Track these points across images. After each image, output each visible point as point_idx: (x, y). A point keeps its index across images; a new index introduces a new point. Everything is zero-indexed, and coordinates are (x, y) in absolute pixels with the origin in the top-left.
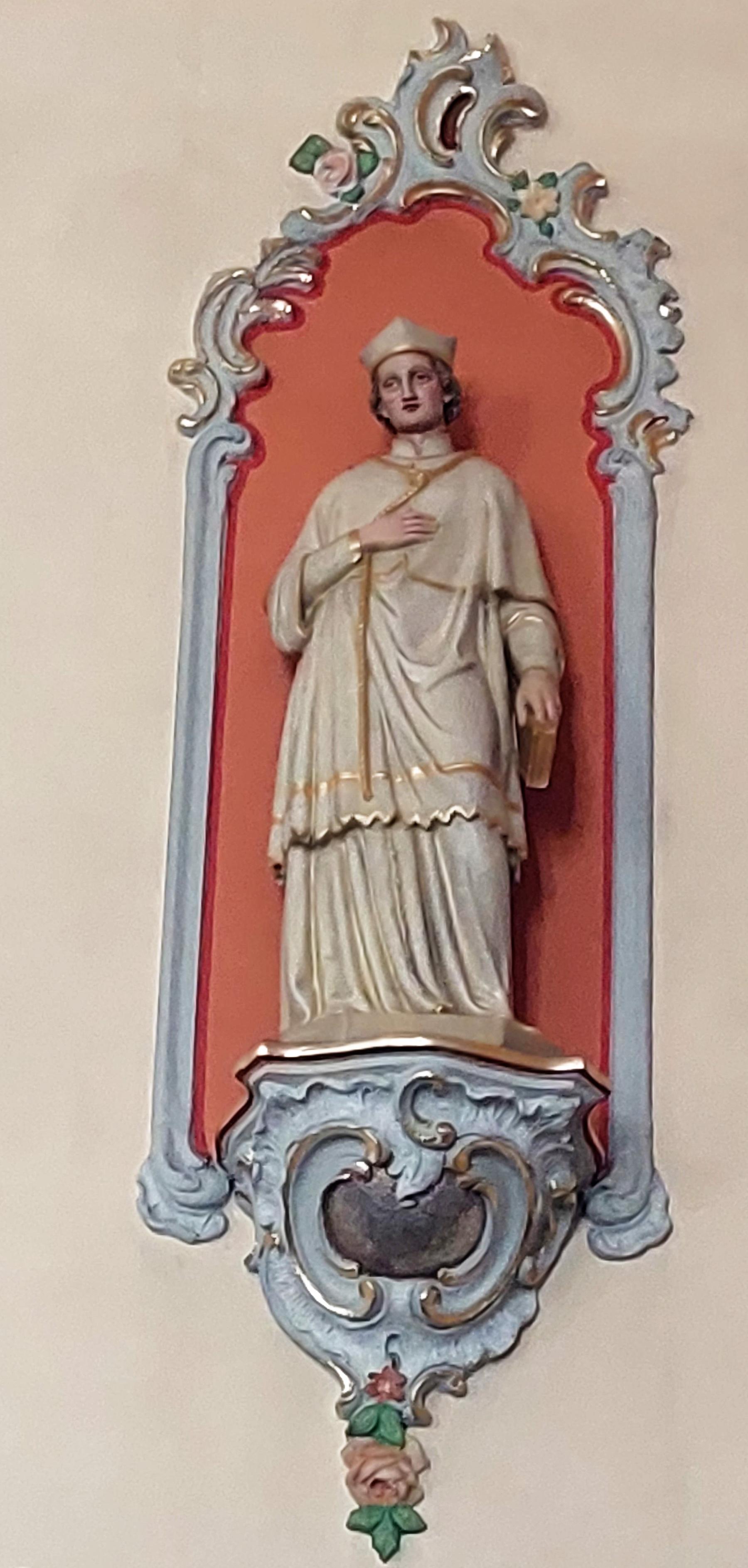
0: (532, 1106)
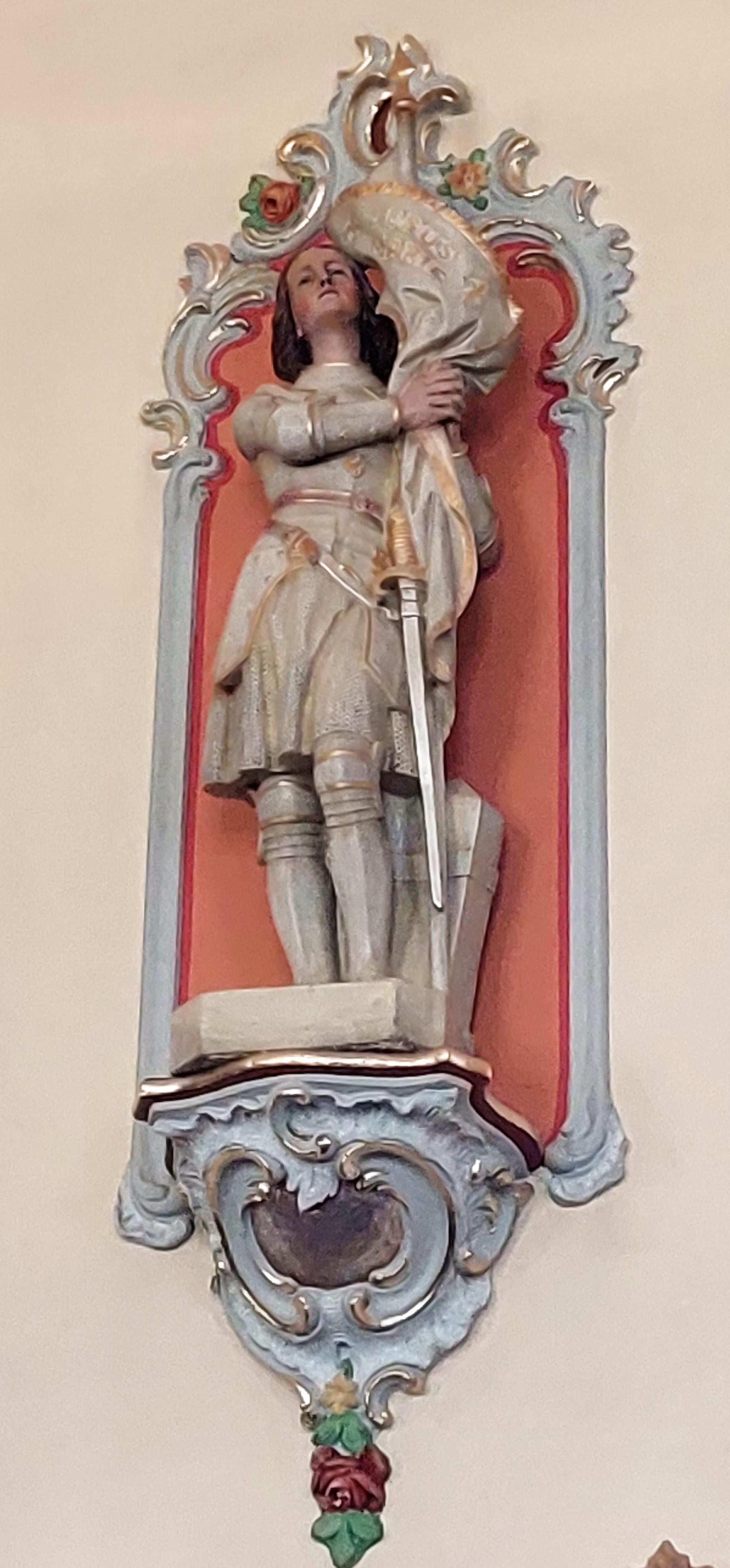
0: (405, 1105)
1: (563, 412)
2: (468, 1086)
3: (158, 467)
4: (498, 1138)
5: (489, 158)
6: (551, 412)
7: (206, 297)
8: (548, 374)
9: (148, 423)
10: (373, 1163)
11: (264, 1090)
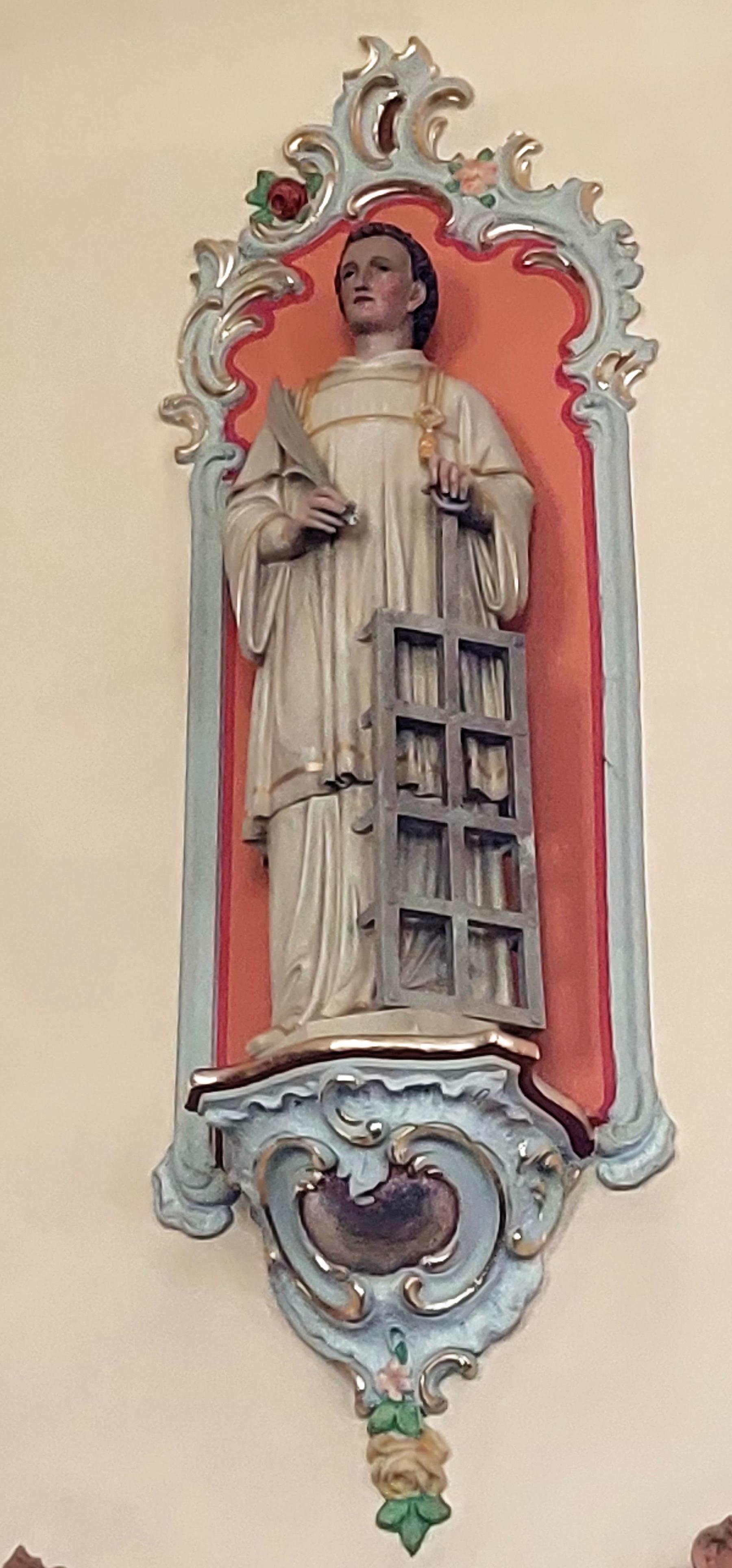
0: (452, 1088)
1: (587, 407)
2: (516, 1068)
3: (180, 462)
4: (543, 1119)
5: (496, 159)
6: (574, 408)
7: (218, 293)
8: (568, 369)
9: (167, 419)
10: (430, 1146)
11: (314, 1077)
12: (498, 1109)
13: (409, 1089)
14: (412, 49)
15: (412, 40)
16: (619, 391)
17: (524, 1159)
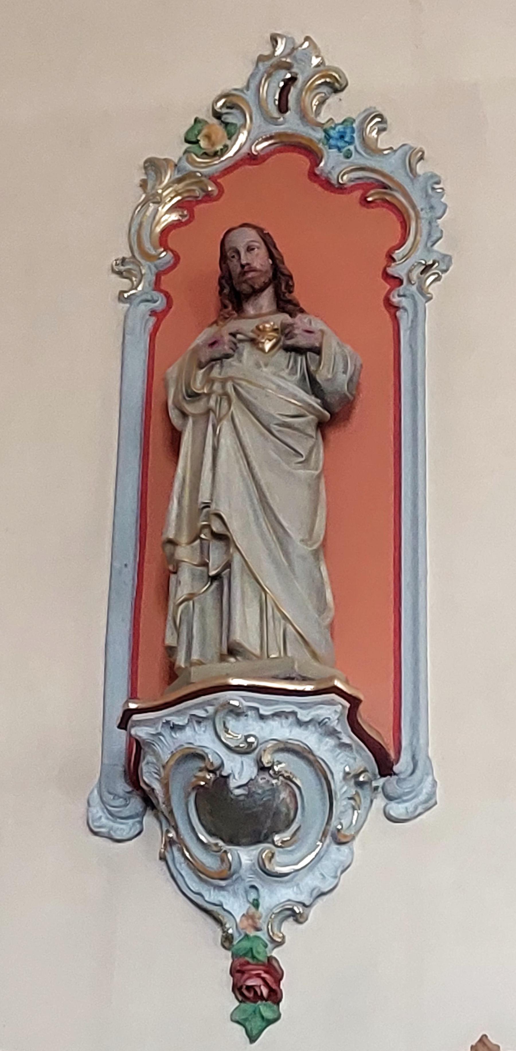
1: (399, 296)
2: (348, 705)
8: (390, 271)
11: (210, 703)
12: (333, 733)
13: (277, 715)
14: (306, 44)
15: (307, 39)
16: (422, 291)
17: (348, 773)
